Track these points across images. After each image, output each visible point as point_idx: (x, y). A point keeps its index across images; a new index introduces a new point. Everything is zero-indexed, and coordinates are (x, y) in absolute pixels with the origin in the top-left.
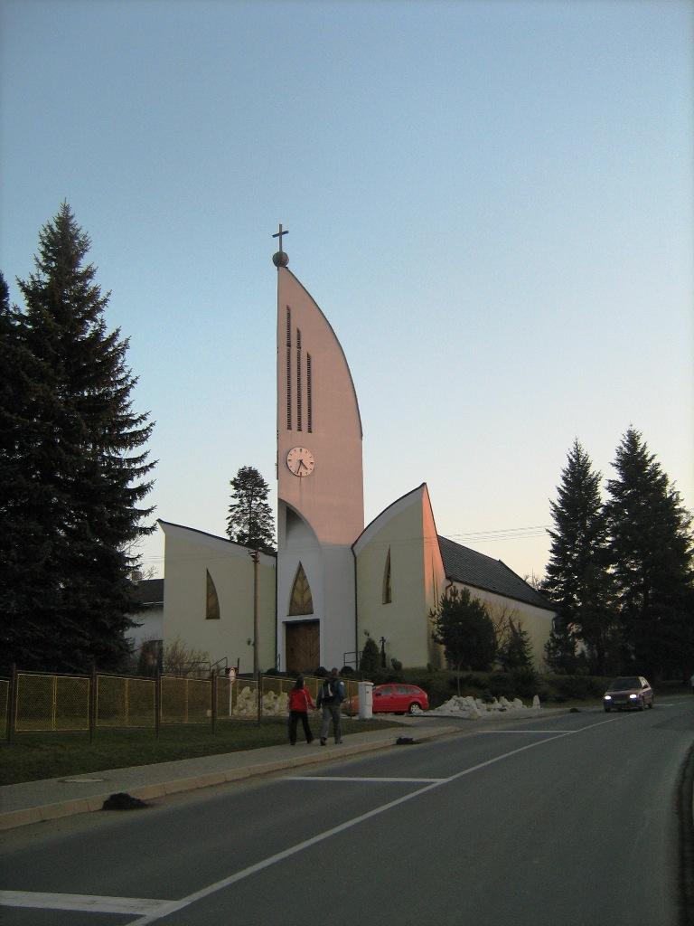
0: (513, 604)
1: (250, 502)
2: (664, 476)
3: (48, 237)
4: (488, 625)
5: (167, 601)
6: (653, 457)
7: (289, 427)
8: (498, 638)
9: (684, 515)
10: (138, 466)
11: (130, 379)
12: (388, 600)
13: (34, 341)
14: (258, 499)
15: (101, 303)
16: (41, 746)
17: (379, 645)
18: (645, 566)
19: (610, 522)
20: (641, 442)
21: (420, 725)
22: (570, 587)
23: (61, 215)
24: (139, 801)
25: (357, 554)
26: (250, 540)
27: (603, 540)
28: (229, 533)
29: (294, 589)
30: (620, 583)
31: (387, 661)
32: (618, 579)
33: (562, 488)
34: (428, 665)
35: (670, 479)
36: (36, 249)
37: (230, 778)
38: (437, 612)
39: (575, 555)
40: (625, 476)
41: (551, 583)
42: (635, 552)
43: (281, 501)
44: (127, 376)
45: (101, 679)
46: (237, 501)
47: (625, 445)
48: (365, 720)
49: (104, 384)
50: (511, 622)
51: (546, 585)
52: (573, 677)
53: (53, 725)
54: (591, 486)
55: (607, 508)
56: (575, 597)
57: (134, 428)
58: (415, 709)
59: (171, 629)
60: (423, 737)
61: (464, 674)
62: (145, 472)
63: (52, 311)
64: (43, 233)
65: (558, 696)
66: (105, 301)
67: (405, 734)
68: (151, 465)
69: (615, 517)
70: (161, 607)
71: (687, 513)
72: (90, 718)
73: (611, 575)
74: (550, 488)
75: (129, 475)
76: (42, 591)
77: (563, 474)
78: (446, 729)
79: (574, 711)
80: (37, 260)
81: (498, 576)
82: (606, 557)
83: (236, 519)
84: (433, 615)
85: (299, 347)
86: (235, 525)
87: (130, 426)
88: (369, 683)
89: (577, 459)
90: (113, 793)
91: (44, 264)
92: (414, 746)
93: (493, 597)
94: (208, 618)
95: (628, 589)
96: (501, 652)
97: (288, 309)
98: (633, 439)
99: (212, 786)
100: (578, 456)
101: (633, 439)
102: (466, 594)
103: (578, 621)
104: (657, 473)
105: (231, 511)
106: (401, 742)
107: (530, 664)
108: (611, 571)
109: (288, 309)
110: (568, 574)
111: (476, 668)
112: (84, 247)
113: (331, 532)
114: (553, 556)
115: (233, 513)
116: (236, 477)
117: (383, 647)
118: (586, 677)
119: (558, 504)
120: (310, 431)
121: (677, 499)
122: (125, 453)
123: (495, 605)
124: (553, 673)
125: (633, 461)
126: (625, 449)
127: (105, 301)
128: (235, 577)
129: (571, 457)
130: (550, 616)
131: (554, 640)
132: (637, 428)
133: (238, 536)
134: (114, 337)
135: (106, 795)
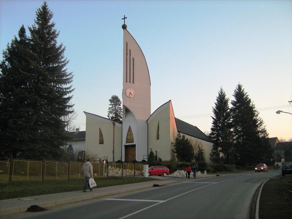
0: (199, 140)
1: (115, 107)
2: (250, 100)
3: (39, 12)
4: (191, 147)
5: (87, 138)
6: (246, 93)
7: (127, 82)
8: (194, 151)
9: (256, 112)
10: (68, 90)
11: (66, 61)
12: (158, 138)
13: (33, 48)
14: (118, 106)
15: (57, 35)
16: (22, 186)
17: (155, 153)
18: (243, 129)
19: (232, 114)
20: (242, 88)
21: (165, 180)
22: (218, 135)
23: (43, 5)
24: (42, 208)
25: (148, 123)
26: (115, 119)
27: (229, 120)
28: (109, 117)
29: (128, 134)
30: (235, 134)
31: (157, 158)
32: (234, 133)
33: (216, 103)
34: (171, 160)
35: (252, 100)
36: (35, 17)
37: (84, 199)
38: (174, 143)
39: (220, 125)
40: (237, 99)
41: (212, 134)
42: (240, 124)
43: (123, 106)
44: (65, 60)
45: (47, 163)
46: (111, 106)
47: (237, 89)
48: (146, 178)
49: (57, 62)
50: (199, 146)
51: (210, 134)
52: (218, 164)
53: (28, 178)
54: (226, 102)
55: (231, 110)
56: (220, 138)
57: (67, 77)
58: (165, 174)
59: (90, 147)
60: (163, 184)
61: (182, 163)
62: (71, 92)
63: (40, 38)
64: (37, 11)
65: (213, 170)
66: (58, 34)
67: (157, 183)
68: (73, 90)
69: (237, 116)
70: (84, 140)
71: (257, 112)
72: (42, 175)
73: (232, 132)
74: (212, 103)
75: (66, 93)
76: (33, 132)
77: (217, 98)
78: (174, 181)
79: (218, 176)
80: (35, 20)
81: (195, 132)
82: (230, 126)
83: (111, 112)
84: (172, 144)
85: (130, 55)
86: (110, 114)
87: (66, 77)
88: (147, 165)
89: (222, 94)
90: (32, 205)
91: (37, 21)
92: (160, 187)
93: (193, 138)
94: (99, 144)
95: (237, 136)
96: (195, 156)
97: (127, 43)
98: (240, 87)
99: (76, 202)
100: (222, 93)
101: (240, 87)
102: (184, 137)
103: (221, 146)
104: (247, 99)
105: (109, 109)
106: (155, 186)
107: (205, 160)
108: (232, 130)
109: (127, 43)
110: (218, 131)
111: (186, 161)
112: (51, 16)
113: (140, 116)
114: (213, 125)
115: (110, 110)
116: (111, 98)
117: (156, 154)
118: (223, 164)
119: (215, 108)
120: (133, 83)
121: (254, 107)
122: (64, 86)
123: (193, 141)
124: (212, 163)
125: (240, 95)
126: (237, 90)
127: (58, 34)
128: (108, 131)
129: (219, 93)
130: (211, 144)
131: (213, 152)
132: (241, 84)
133: (111, 118)
134: (61, 46)
135: (29, 206)
